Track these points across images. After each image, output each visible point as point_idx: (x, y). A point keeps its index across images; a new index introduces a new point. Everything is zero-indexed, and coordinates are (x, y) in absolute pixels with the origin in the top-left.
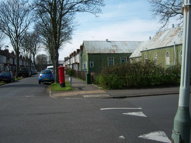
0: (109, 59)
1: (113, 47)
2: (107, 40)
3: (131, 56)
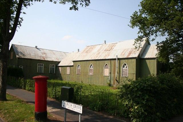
0: (39, 65)
1: (43, 54)
2: (36, 47)
3: (60, 65)
